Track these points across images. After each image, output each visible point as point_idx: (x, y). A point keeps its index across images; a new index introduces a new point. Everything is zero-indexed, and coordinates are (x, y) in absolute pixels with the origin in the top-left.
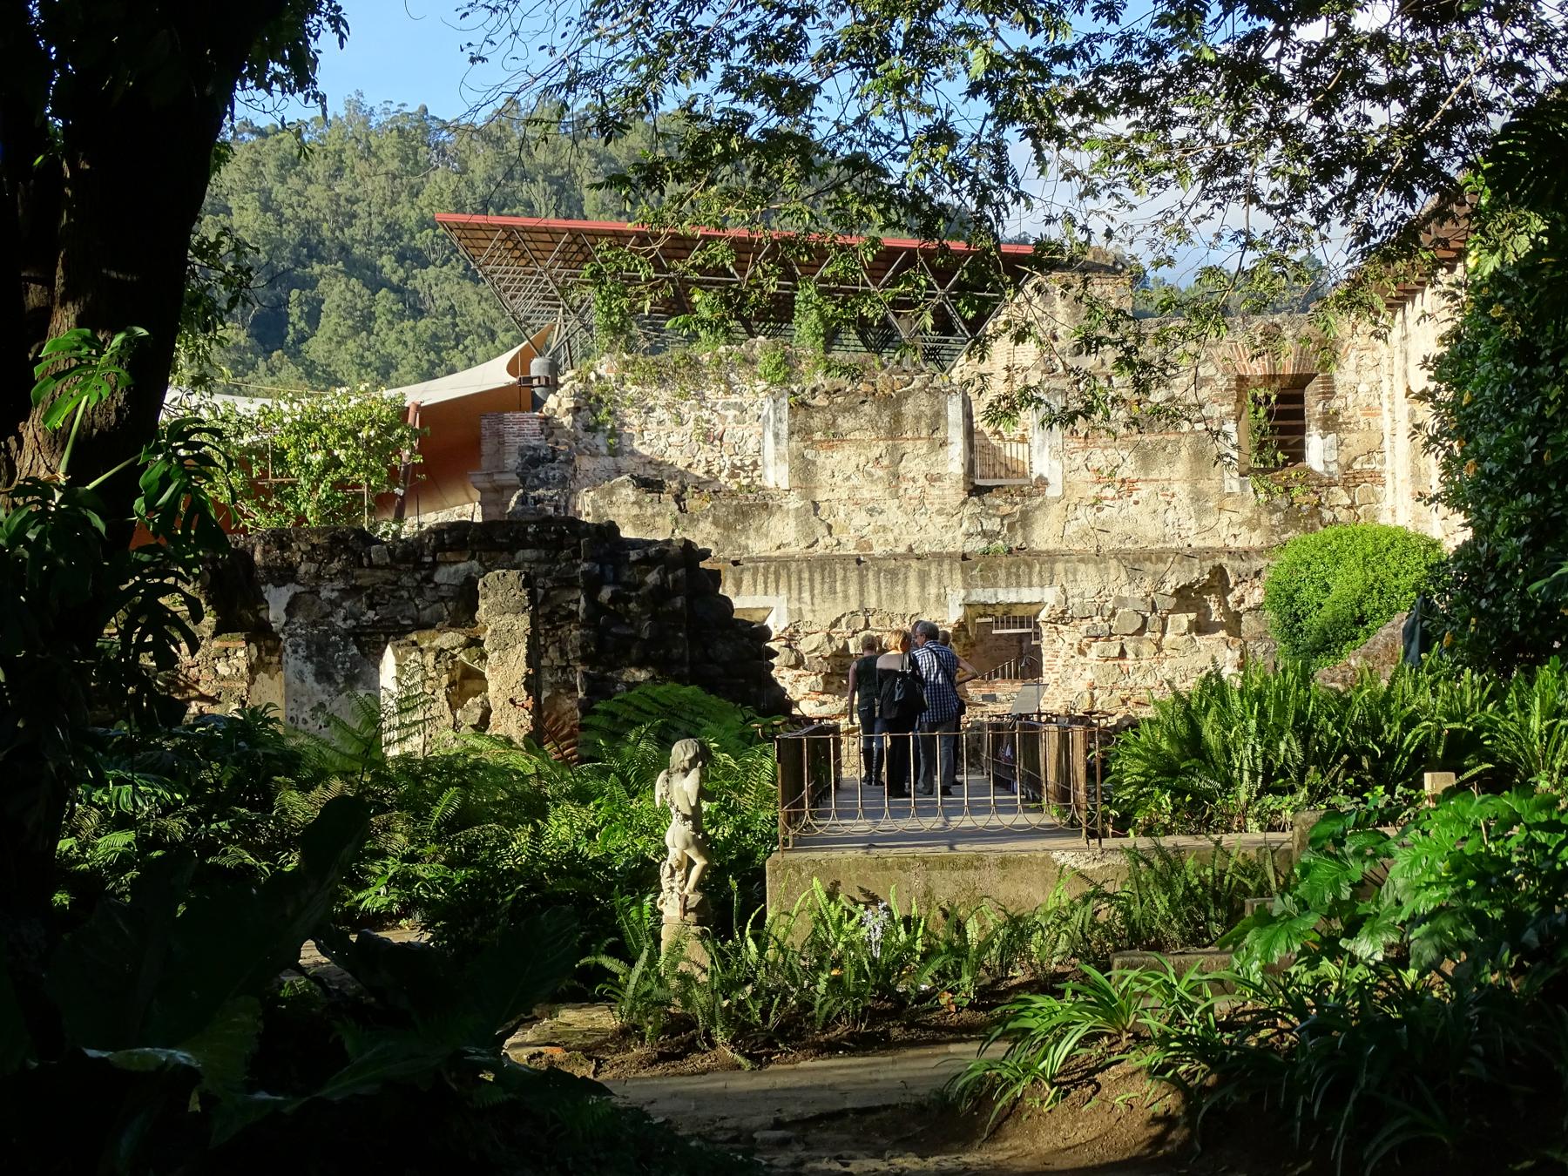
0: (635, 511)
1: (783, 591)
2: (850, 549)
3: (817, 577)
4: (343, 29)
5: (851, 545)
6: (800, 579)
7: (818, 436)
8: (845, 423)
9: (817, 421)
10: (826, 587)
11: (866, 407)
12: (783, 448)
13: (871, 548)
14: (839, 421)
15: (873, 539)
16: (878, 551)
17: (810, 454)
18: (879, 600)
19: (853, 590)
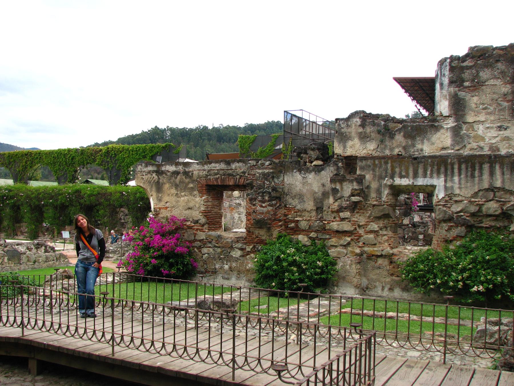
0: (361, 130)
1: (442, 176)
2: (486, 151)
3: (463, 166)
4: (471, 88)
5: (486, 149)
6: (338, 371)
7: (467, 84)
8: (484, 74)
9: (467, 75)
10: (469, 174)
11: (499, 65)
12: (445, 92)
13: (498, 150)
14: (481, 74)
15: (500, 146)
16: (503, 152)
17: (462, 94)
18: (503, 182)
19: (486, 176)
